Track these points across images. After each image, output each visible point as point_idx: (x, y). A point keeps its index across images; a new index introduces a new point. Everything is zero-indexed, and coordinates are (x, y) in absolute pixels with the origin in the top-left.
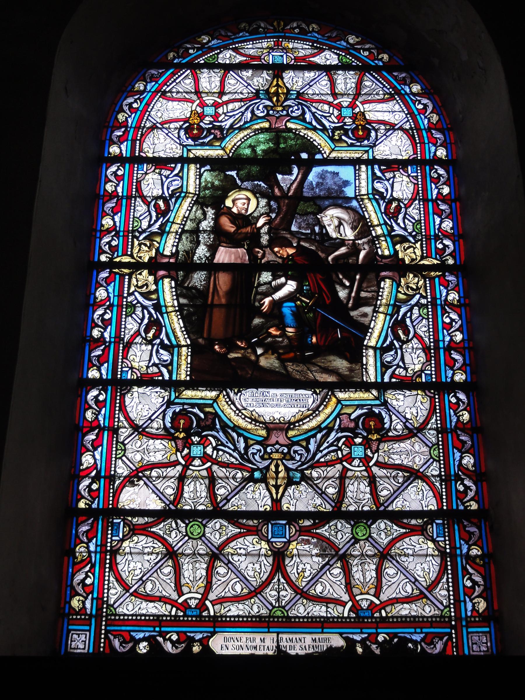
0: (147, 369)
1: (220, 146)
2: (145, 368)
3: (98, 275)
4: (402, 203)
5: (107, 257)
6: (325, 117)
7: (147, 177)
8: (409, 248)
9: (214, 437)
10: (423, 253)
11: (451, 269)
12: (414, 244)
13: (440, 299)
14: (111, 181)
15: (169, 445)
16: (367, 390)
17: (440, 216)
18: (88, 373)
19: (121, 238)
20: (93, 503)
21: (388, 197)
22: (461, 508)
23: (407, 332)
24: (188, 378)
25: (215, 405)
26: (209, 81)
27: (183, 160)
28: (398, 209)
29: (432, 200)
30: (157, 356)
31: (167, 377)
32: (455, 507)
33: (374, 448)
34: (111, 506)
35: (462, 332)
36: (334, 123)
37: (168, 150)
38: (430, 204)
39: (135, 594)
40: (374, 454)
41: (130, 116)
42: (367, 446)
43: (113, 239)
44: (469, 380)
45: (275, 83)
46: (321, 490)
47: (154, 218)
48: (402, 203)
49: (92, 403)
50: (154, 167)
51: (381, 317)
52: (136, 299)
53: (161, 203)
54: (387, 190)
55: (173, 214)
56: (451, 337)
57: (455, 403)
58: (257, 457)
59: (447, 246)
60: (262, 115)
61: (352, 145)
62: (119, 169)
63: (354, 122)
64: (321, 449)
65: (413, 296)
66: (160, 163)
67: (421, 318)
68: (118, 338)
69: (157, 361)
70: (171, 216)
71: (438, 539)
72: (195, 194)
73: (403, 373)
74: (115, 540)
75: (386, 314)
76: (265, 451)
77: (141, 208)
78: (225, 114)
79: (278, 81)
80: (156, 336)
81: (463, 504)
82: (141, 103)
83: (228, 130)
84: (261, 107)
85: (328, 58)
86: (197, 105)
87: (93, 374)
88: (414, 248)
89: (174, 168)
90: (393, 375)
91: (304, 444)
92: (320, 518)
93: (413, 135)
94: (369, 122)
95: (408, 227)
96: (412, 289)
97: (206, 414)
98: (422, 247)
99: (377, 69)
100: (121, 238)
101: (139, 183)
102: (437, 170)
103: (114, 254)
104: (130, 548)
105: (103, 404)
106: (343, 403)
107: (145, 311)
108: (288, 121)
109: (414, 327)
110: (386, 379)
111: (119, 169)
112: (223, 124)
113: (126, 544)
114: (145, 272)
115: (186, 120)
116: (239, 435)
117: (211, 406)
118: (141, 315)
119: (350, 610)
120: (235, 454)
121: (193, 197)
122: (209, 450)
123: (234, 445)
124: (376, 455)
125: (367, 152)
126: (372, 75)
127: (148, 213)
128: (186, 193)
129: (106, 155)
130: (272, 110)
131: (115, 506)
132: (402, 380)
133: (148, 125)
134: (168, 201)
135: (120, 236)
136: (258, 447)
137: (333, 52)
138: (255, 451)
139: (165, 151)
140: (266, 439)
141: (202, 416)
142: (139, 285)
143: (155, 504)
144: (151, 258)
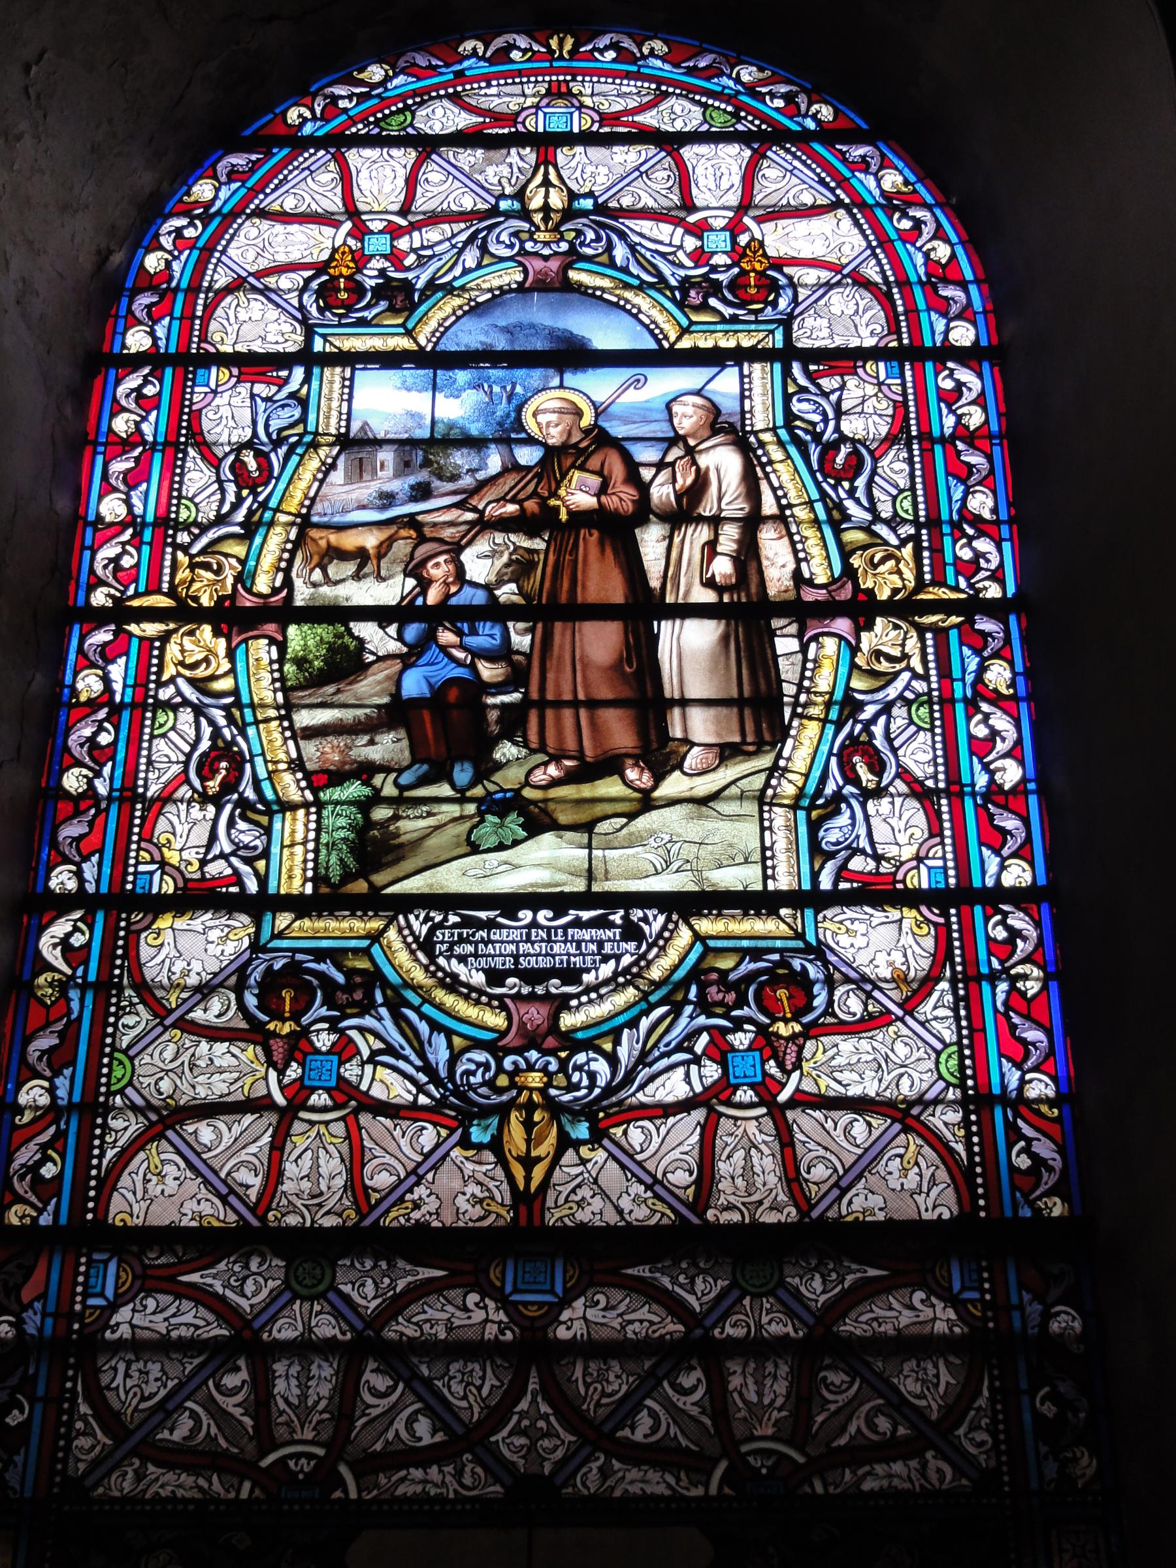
0: (201, 868)
1: (403, 325)
2: (196, 865)
3: (82, 639)
4: (195, 790)
5: (108, 595)
6: (663, 255)
7: (217, 401)
8: (194, 666)
9: (681, 266)
10: (162, 650)
11: (995, 609)
12: (898, 548)
13: (963, 680)
14: (125, 410)
15: (250, 1053)
16: (773, 912)
17: (963, 481)
18: (48, 878)
19: (146, 550)
20: (40, 1212)
21: (229, 807)
22: (1026, 1212)
23: (878, 767)
24: (309, 889)
25: (376, 950)
26: (380, 176)
27: (812, 900)
28: (206, 768)
29: (942, 440)
30: (229, 834)
31: (252, 886)
32: (1008, 1213)
33: (790, 1060)
34: (90, 1216)
35: (1021, 762)
36: (362, 1030)
37: (270, 338)
38: (938, 449)
39: (260, 1212)
40: (788, 1073)
41: (176, 258)
42: (768, 1052)
43: (125, 552)
44: (1042, 881)
45: (538, 1172)
46: (654, 1177)
47: (231, 498)
48: (195, 790)
49: (54, 957)
50: (900, 876)
51: (813, 728)
52: (179, 693)
53: (866, 776)
54: (826, 420)
55: (282, 486)
56: (991, 773)
57: (1004, 942)
58: (590, 235)
59: (983, 555)
60: (507, 253)
61: (734, 319)
62: (146, 382)
63: (305, 1032)
64: (650, 1058)
65: (203, 552)
66: (880, 893)
67: (913, 729)
68: (128, 794)
69: (228, 849)
70: (271, 492)
71: (968, 1295)
72: (771, 804)
73: (260, 388)
74: (95, 1307)
75: (825, 721)
76: (500, 1069)
77: (197, 476)
78: (697, 1060)
79: (528, 1179)
80: (230, 786)
81: (1031, 1204)
82: (205, 227)
83: (422, 291)
84: (504, 237)
85: (679, 114)
86: (349, 234)
87: (62, 879)
88: (898, 561)
89: (286, 381)
90: (842, 872)
91: (608, 1047)
92: (203, 1244)
93: (889, 295)
94: (778, 264)
95: (880, 507)
96: (891, 659)
97: (350, 973)
98: (161, 667)
99: (802, 139)
100: (146, 550)
101: (935, 831)
102: (952, 371)
103: (127, 588)
104: (133, 1327)
105: (83, 953)
106: (711, 943)
107: (203, 721)
108: (503, 1034)
109: (894, 751)
110: (826, 883)
111: (146, 382)
112: (410, 275)
113: (124, 1314)
114: (884, 595)
115: (321, 268)
116: (435, 1026)
117: (366, 952)
118: (192, 733)
119: (723, 1481)
120: (637, 239)
121: (775, 795)
122: (691, 243)
123: (422, 1055)
124: (796, 1075)
125: (280, 936)
126: (788, 151)
127: (896, 744)
128: (316, 434)
129: (117, 349)
130: (531, 239)
131: (100, 1216)
132: (865, 884)
133: (222, 281)
134: (266, 456)
135: (142, 543)
136: (480, 1056)
137: (693, 100)
138: (473, 1067)
139: (264, 339)
140: (569, 266)
141: (340, 978)
142: (188, 661)
143: (197, 1207)
144: (870, 627)
